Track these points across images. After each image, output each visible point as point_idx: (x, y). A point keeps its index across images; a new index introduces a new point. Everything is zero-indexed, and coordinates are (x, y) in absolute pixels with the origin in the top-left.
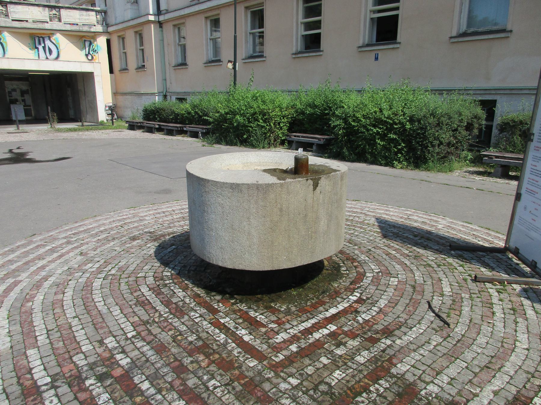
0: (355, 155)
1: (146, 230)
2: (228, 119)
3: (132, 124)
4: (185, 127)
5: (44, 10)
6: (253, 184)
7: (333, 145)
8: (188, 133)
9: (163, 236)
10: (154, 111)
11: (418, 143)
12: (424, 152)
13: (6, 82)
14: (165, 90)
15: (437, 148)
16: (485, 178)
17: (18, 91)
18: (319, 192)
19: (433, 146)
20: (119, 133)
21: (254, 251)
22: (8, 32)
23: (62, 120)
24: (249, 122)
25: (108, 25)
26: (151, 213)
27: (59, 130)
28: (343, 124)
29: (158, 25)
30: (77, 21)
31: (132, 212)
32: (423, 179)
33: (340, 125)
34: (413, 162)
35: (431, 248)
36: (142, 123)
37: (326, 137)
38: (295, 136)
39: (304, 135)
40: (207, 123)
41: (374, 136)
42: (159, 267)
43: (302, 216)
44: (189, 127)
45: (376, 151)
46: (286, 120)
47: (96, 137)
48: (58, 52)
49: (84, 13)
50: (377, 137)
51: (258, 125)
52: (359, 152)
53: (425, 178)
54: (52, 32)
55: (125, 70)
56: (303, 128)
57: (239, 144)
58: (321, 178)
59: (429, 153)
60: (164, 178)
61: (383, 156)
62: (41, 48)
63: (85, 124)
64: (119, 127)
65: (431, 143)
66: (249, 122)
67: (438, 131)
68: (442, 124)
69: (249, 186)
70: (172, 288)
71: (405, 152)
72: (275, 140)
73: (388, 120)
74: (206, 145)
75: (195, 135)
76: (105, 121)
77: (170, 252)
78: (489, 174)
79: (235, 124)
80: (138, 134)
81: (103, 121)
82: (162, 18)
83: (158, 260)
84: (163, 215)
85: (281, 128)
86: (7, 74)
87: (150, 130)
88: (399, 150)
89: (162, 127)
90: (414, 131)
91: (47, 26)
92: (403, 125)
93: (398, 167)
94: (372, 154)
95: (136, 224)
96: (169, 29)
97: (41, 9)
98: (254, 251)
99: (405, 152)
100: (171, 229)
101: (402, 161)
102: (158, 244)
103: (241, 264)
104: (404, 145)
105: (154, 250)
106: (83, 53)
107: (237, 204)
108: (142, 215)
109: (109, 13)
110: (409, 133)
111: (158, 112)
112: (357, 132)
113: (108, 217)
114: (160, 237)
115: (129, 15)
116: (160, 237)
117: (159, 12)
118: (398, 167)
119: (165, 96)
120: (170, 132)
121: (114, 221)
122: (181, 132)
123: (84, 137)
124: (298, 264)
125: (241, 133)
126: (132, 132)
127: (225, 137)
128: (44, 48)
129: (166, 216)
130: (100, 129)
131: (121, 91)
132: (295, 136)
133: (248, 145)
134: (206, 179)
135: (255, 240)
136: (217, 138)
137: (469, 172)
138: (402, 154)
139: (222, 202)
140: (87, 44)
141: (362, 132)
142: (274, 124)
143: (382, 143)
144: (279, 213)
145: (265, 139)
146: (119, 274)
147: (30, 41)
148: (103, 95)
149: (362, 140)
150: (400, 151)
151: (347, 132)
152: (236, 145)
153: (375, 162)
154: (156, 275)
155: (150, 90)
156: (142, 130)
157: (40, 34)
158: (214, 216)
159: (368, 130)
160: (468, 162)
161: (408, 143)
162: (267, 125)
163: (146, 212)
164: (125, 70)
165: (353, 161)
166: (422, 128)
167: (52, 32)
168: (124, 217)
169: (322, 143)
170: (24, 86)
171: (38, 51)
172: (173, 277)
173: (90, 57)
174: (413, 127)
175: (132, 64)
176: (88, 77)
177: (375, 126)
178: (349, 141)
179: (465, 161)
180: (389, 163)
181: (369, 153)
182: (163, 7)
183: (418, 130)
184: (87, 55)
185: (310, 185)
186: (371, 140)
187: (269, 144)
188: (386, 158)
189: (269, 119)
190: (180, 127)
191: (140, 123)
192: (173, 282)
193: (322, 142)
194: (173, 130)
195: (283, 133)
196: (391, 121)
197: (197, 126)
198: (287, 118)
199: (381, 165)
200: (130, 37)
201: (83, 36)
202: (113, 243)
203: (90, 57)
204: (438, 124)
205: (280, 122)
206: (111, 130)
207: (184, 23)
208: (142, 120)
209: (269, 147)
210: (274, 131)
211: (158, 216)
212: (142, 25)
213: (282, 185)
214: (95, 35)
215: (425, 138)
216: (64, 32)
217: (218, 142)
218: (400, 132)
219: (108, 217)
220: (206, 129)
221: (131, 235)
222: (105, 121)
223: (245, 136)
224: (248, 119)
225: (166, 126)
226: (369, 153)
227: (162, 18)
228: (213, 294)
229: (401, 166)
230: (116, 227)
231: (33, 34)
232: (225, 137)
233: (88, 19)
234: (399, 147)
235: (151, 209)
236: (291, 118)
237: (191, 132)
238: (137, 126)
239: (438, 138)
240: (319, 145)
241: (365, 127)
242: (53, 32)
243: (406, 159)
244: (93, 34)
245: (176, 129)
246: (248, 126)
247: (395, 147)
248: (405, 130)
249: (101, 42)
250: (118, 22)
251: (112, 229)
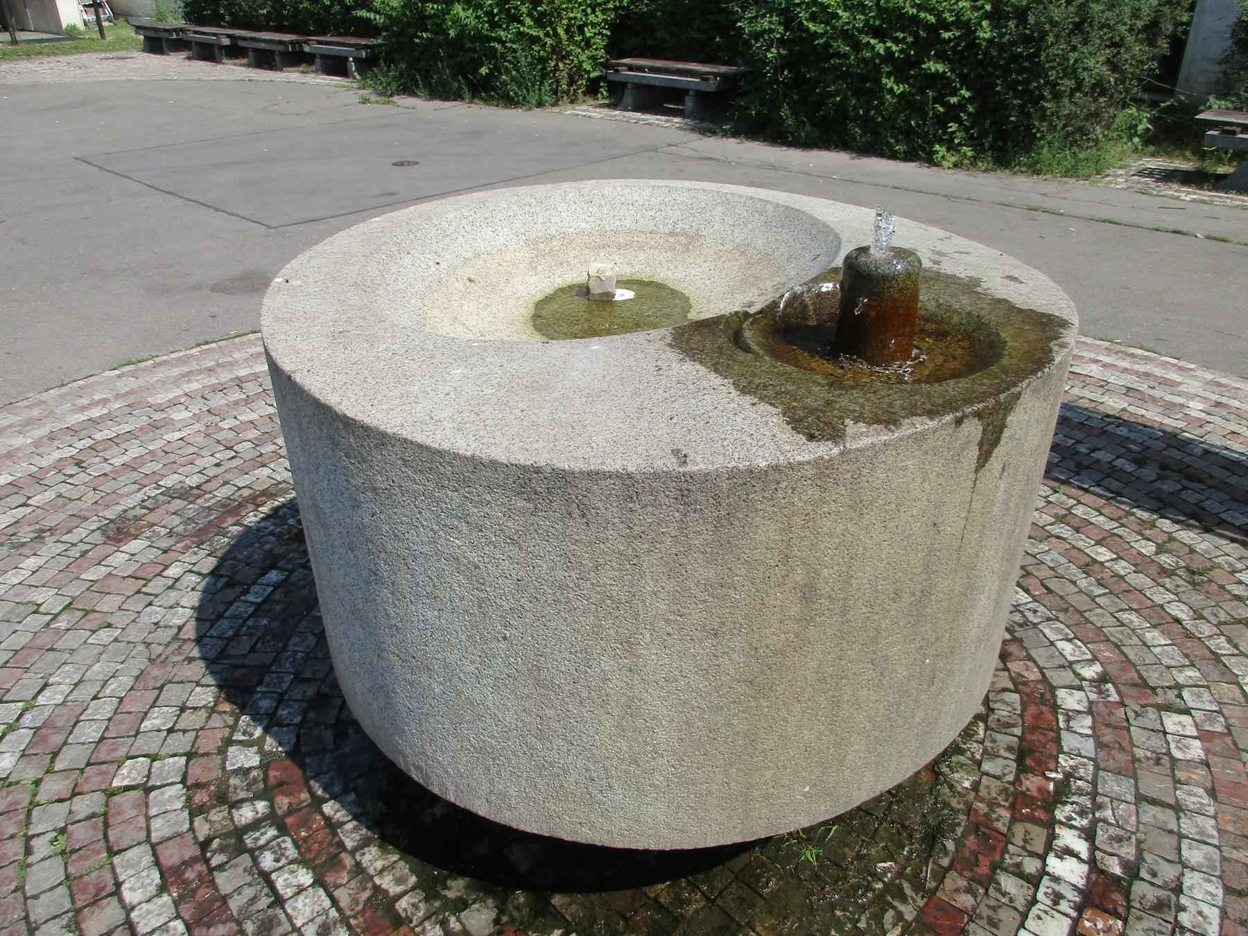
0: (814, 125)
1: (169, 482)
2: (431, 17)
4: (306, 42)
6: (656, 476)
7: (746, 94)
8: (318, 61)
9: (232, 508)
11: (1012, 86)
12: (1029, 116)
15: (1066, 101)
16: (1206, 195)
19: (1057, 96)
20: (119, 63)
21: (658, 778)
24: (494, 25)
26: (195, 386)
28: (781, 29)
31: (125, 385)
32: (1033, 205)
33: (771, 31)
34: (991, 148)
35: (1222, 523)
36: (182, 30)
37: (723, 69)
38: (631, 68)
39: (658, 64)
40: (367, 28)
41: (878, 68)
42: (212, 710)
43: (906, 599)
44: (319, 42)
45: (879, 113)
46: (601, 17)
47: (49, 79)
50: (887, 69)
51: (520, 34)
52: (825, 118)
53: (1036, 200)
56: (649, 42)
57: (467, 96)
59: (1043, 118)
60: (247, 224)
61: (901, 131)
63: (22, 36)
64: (121, 44)
65: (1055, 85)
66: (494, 25)
67: (1074, 49)
68: (1091, 25)
69: (631, 487)
70: (267, 861)
71: (970, 114)
72: (572, 82)
73: (922, 15)
74: (373, 98)
75: (336, 67)
76: (81, 26)
77: (258, 610)
78: (1219, 183)
79: (452, 33)
80: (175, 65)
81: (74, 28)
83: (211, 662)
84: (237, 395)
85: (588, 44)
87: (207, 53)
88: (950, 108)
89: (241, 43)
90: (1002, 48)
92: (968, 29)
93: (945, 164)
94: (866, 122)
95: (135, 451)
98: (658, 778)
99: (970, 114)
100: (265, 472)
101: (960, 144)
102: (209, 564)
103: (592, 825)
104: (967, 95)
105: (194, 599)
107: (560, 574)
108: (161, 398)
110: (985, 54)
112: (826, 53)
113: (35, 412)
114: (222, 518)
116: (222, 518)
118: (945, 164)
120: (265, 60)
121: (52, 437)
122: (296, 58)
123: (13, 80)
125: (472, 60)
126: (155, 60)
127: (427, 76)
129: (247, 401)
130: (66, 53)
132: (631, 68)
133: (493, 98)
134: (366, 429)
135: (662, 736)
136: (401, 75)
137: (1150, 173)
138: (960, 122)
139: (473, 556)
141: (837, 55)
142: (567, 31)
143: (899, 89)
144: (795, 610)
145: (544, 76)
146: (31, 774)
149: (838, 78)
150: (953, 113)
151: (791, 53)
152: (458, 96)
153: (873, 147)
154: (197, 771)
156: (184, 55)
158: (431, 614)
159: (857, 47)
160: (1136, 140)
161: (982, 91)
162: (547, 35)
163: (177, 381)
165: (808, 145)
166: (1027, 40)
168: (95, 413)
169: (713, 89)
172: (274, 774)
174: (1001, 35)
177: (880, 34)
178: (798, 82)
179: (1130, 139)
180: (919, 152)
181: (856, 118)
183: (1013, 43)
186: (865, 79)
187: (555, 92)
188: (909, 133)
189: (551, 14)
190: (292, 43)
191: (175, 30)
192: (272, 818)
193: (711, 86)
194: (272, 52)
195: (593, 58)
196: (932, 19)
197: (341, 40)
198: (604, 12)
199: (893, 156)
202: (32, 563)
204: (1078, 27)
205: (585, 25)
206: (94, 56)
208: (181, 23)
209: (555, 104)
210: (569, 54)
211: (218, 401)
213: (823, 469)
215: (1037, 70)
217: (407, 89)
218: (955, 53)
219: (35, 412)
220: (366, 47)
221: (111, 514)
222: (81, 26)
223: (484, 71)
224: (490, 14)
225: (253, 39)
226: (856, 118)
228: (456, 888)
229: (953, 159)
230: (58, 467)
234: (953, 100)
235: (194, 366)
236: (616, 9)
237: (324, 57)
238: (168, 41)
239: (1075, 71)
240: (701, 96)
241: (846, 36)
243: (972, 138)
245: (282, 48)
246: (489, 39)
247: (939, 99)
248: (973, 45)
251: (37, 479)
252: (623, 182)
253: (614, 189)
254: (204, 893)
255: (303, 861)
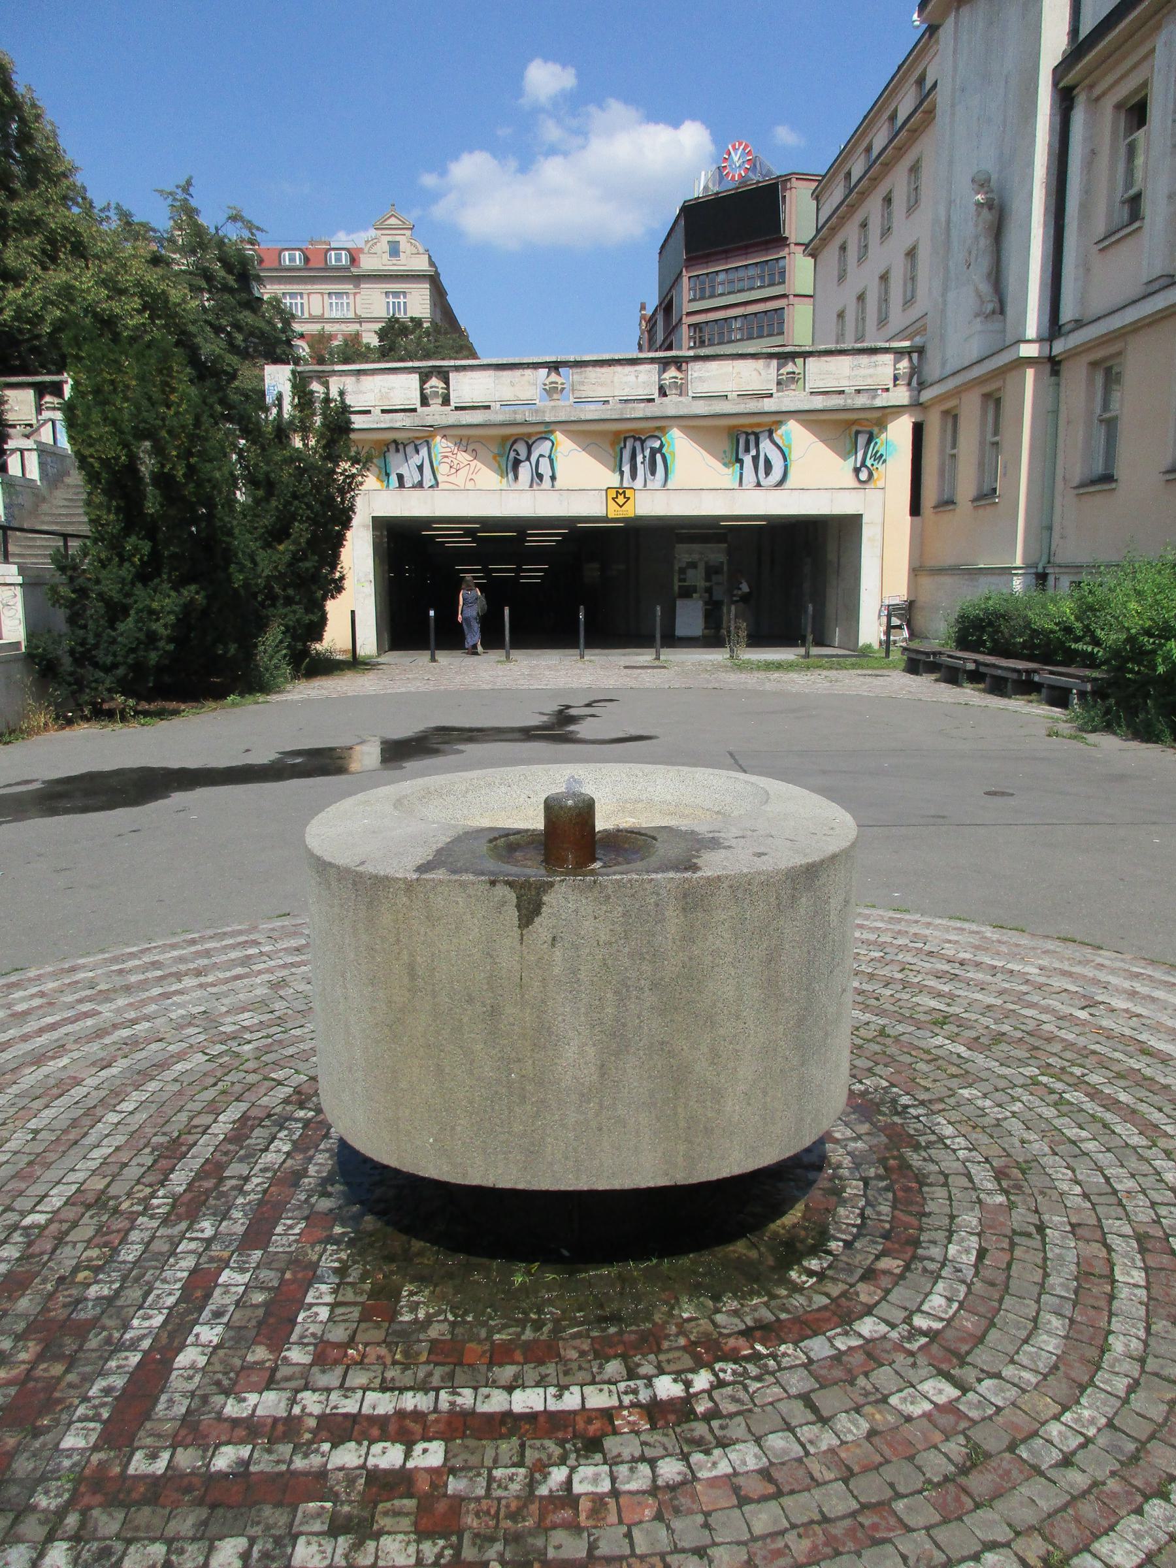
3: (914, 656)
5: (768, 366)
10: (982, 620)
13: (680, 547)
14: (1045, 559)
17: (701, 566)
18: (546, 936)
22: (679, 427)
23: (757, 640)
25: (922, 386)
27: (741, 667)
29: (1047, 368)
30: (843, 384)
44: (1052, 673)
48: (786, 467)
49: (864, 360)
54: (778, 418)
55: (947, 503)
58: (551, 885)
62: (748, 460)
75: (1059, 698)
76: (876, 646)
79: (1161, 669)
80: (925, 686)
81: (869, 646)
82: (1059, 347)
86: (683, 528)
89: (982, 669)
91: (768, 405)
96: (1076, 375)
97: (491, 373)
106: (850, 463)
109: (930, 353)
111: (990, 624)
115: (974, 350)
117: (1054, 328)
119: (1042, 578)
120: (999, 686)
122: (1026, 687)
123: (768, 686)
124: (475, 1178)
127: (1133, 712)
128: (755, 459)
131: (931, 563)
140: (862, 439)
147: (726, 445)
148: (882, 575)
155: (1006, 557)
156: (933, 677)
157: (751, 426)
164: (947, 503)
167: (778, 418)
170: (717, 554)
171: (742, 468)
173: (864, 475)
175: (966, 489)
176: (846, 529)
182: (1067, 313)
184: (857, 471)
185: (504, 903)
190: (1028, 672)
191: (934, 654)
194: (1006, 680)
200: (971, 408)
201: (854, 422)
203: (864, 475)
207: (1119, 354)
212: (1004, 373)
214: (887, 414)
216: (806, 417)
222: (876, 646)
227: (1059, 347)
231: (734, 427)
232: (1133, 712)
233: (877, 376)
242: (781, 417)
244: (542, 428)
245: (1015, 676)
249: (899, 433)
250: (949, 369)
252: (710, 770)
253: (702, 774)
254: (246, 1131)
255: (294, 1143)
